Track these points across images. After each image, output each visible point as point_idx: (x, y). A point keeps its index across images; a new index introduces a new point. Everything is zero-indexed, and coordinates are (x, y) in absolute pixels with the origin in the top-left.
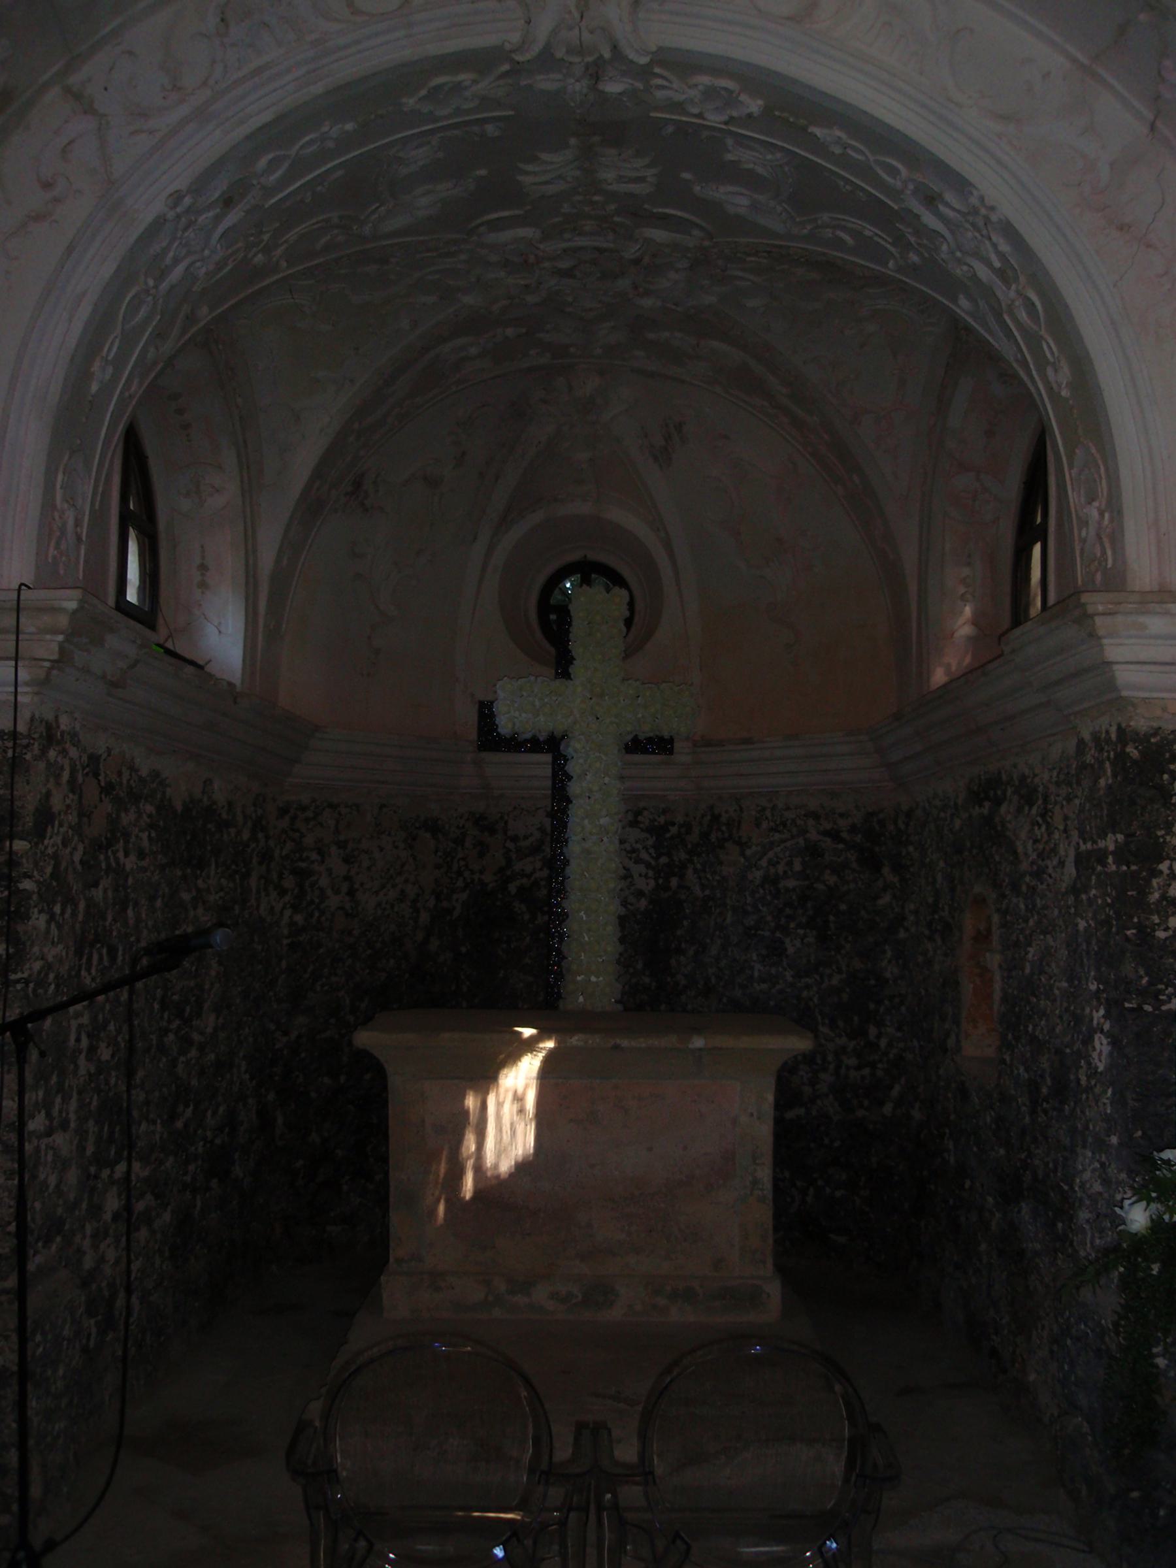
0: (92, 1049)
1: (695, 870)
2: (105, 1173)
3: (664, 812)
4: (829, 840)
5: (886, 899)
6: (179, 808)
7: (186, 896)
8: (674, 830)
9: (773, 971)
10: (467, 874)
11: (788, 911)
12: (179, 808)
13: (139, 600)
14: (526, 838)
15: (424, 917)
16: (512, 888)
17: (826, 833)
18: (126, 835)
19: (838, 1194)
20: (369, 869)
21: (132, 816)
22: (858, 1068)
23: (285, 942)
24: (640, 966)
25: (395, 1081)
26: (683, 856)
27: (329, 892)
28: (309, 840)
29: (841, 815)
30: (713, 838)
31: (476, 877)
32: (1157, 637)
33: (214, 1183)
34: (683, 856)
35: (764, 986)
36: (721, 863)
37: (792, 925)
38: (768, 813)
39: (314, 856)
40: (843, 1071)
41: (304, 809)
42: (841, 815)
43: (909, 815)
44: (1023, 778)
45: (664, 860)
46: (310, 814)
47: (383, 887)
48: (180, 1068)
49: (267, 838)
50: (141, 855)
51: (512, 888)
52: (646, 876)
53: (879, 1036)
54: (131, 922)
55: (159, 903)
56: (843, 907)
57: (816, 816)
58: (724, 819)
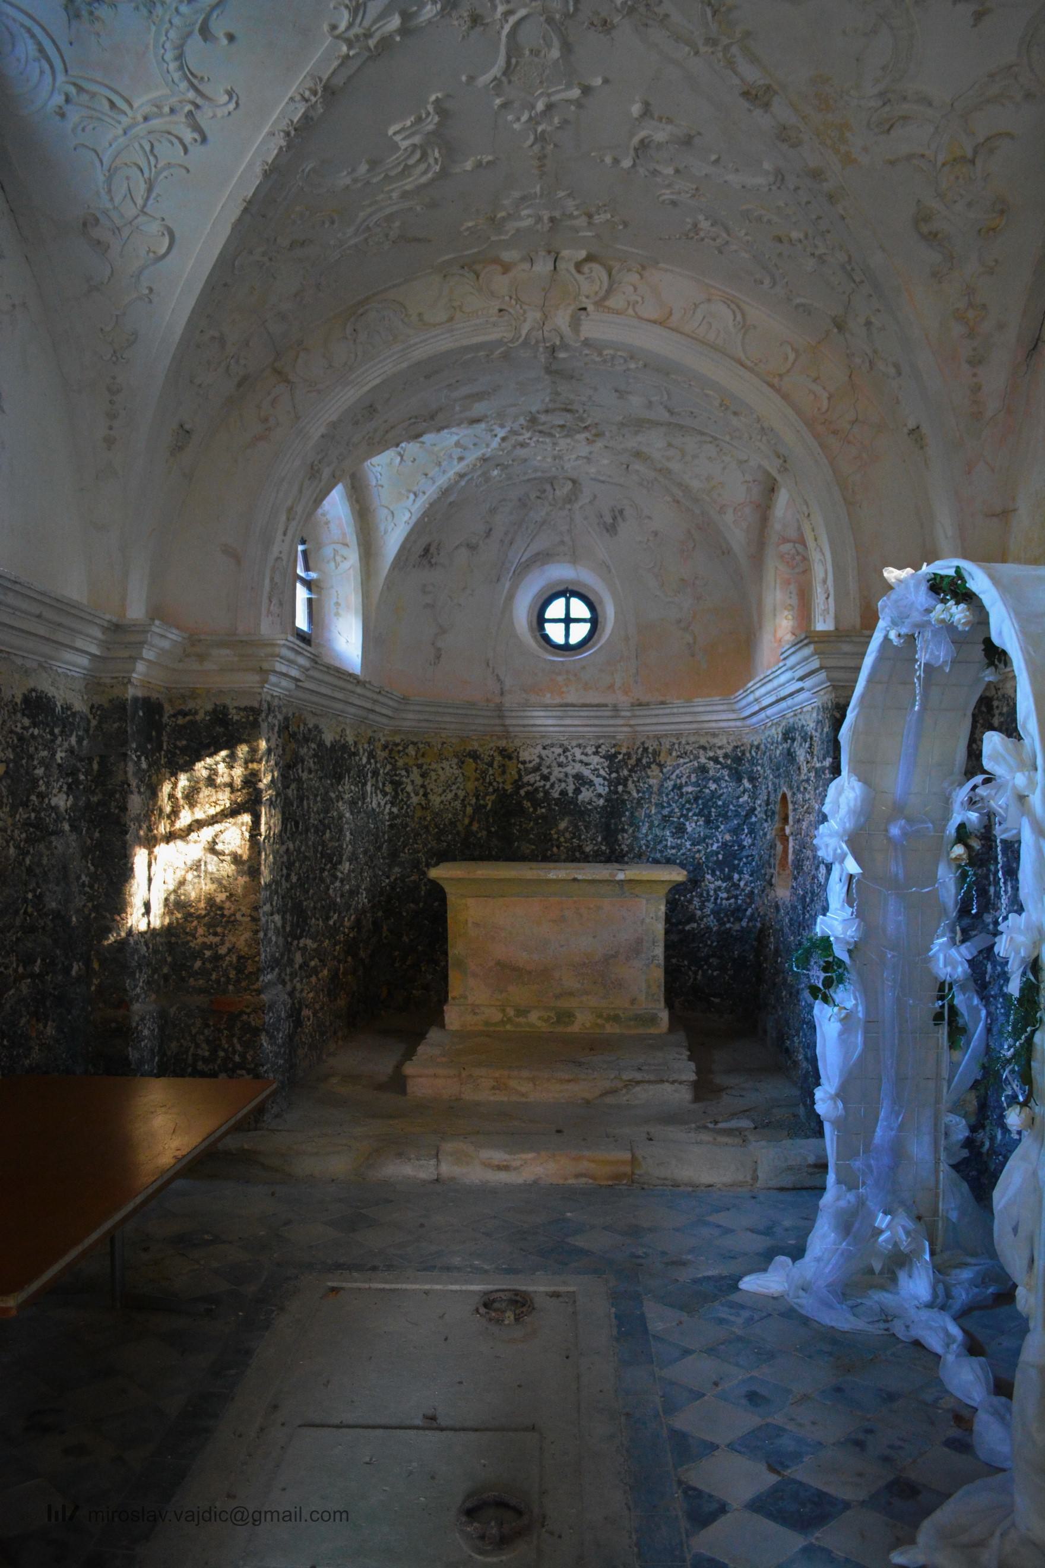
0: (288, 876)
1: (633, 782)
2: (295, 942)
3: (614, 746)
4: (712, 763)
5: (746, 798)
6: (329, 745)
7: (333, 795)
8: (620, 757)
9: (679, 842)
10: (495, 784)
11: (688, 806)
12: (329, 745)
13: (309, 627)
14: (530, 762)
15: (469, 810)
16: (522, 792)
17: (710, 759)
18: (303, 761)
19: (715, 973)
20: (436, 781)
21: (305, 750)
22: (728, 899)
23: (387, 823)
24: (599, 839)
25: (451, 899)
26: (626, 772)
27: (412, 795)
28: (400, 763)
29: (720, 748)
30: (644, 761)
31: (501, 786)
32: (846, 654)
33: (349, 959)
34: (626, 772)
35: (674, 851)
36: (648, 777)
37: (690, 814)
38: (676, 746)
39: (404, 773)
40: (719, 901)
41: (397, 745)
42: (720, 748)
43: (758, 747)
44: (803, 726)
45: (614, 775)
46: (400, 748)
47: (444, 791)
48: (331, 891)
49: (376, 762)
50: (310, 772)
51: (522, 792)
52: (604, 785)
53: (740, 880)
54: (306, 807)
55: (319, 799)
56: (720, 803)
57: (704, 748)
58: (650, 750)
